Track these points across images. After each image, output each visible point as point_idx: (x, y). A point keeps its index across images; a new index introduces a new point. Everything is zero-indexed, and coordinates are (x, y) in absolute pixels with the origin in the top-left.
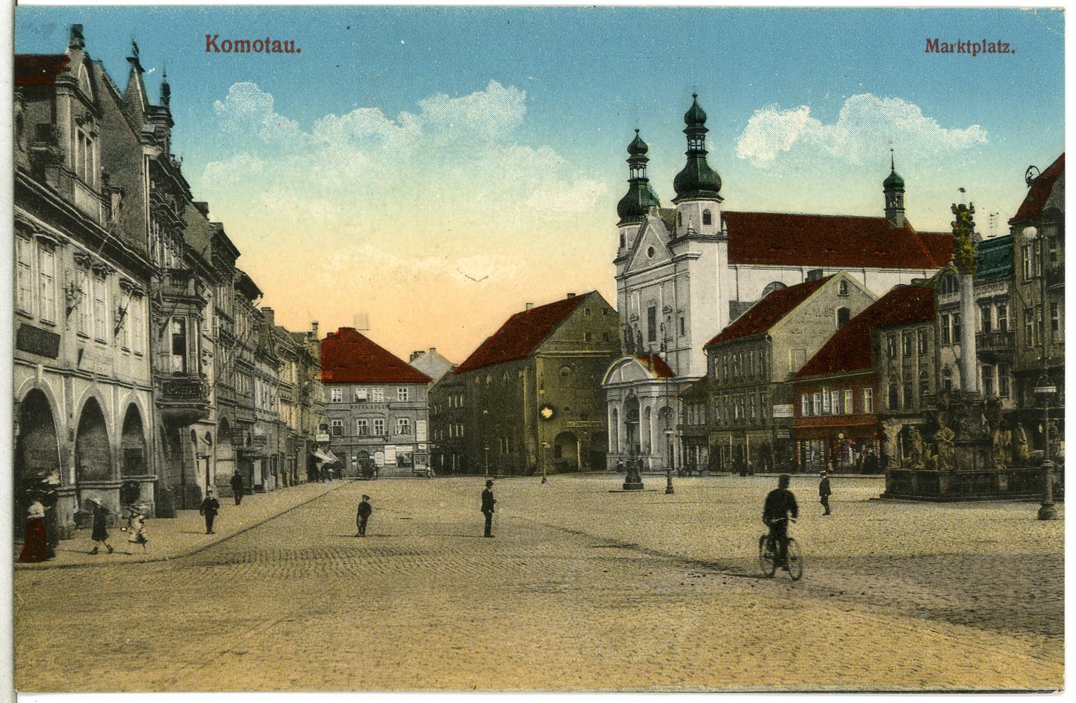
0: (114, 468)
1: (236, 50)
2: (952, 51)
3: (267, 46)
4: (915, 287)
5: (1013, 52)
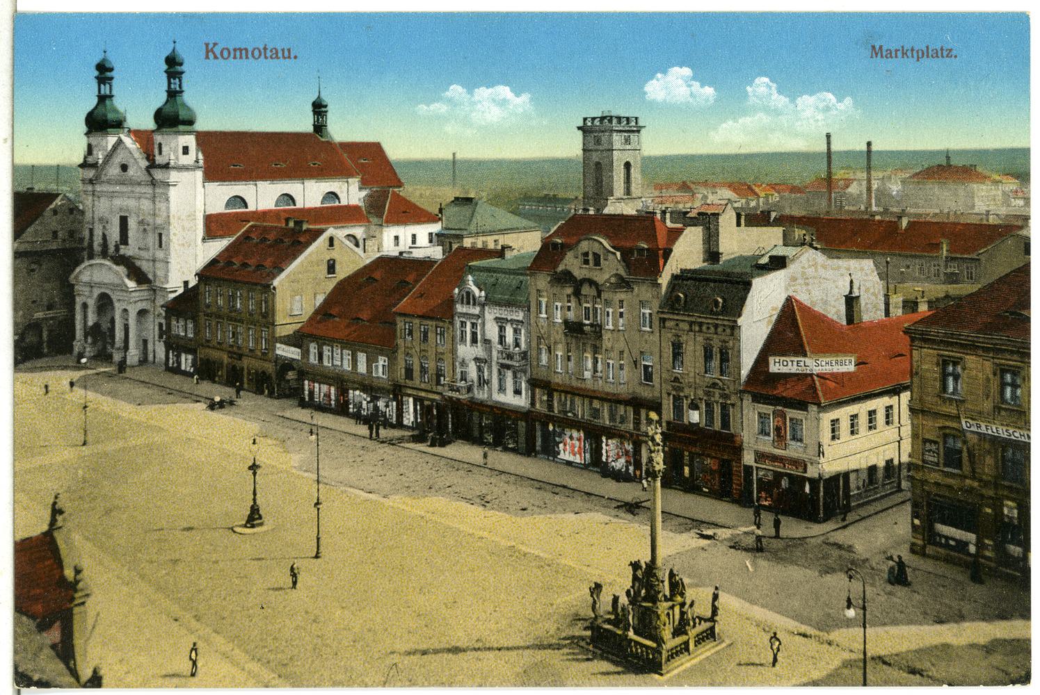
1: (235, 58)
2: (896, 57)
4: (362, 211)
5: (956, 57)
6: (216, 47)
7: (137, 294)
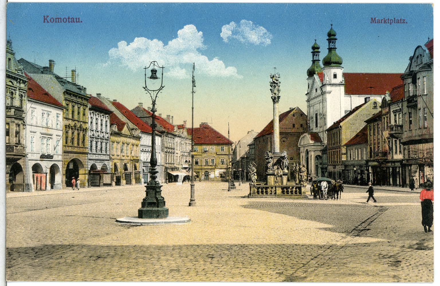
0: (338, 176)
2: (382, 23)
3: (69, 20)
6: (48, 17)
7: (313, 147)
